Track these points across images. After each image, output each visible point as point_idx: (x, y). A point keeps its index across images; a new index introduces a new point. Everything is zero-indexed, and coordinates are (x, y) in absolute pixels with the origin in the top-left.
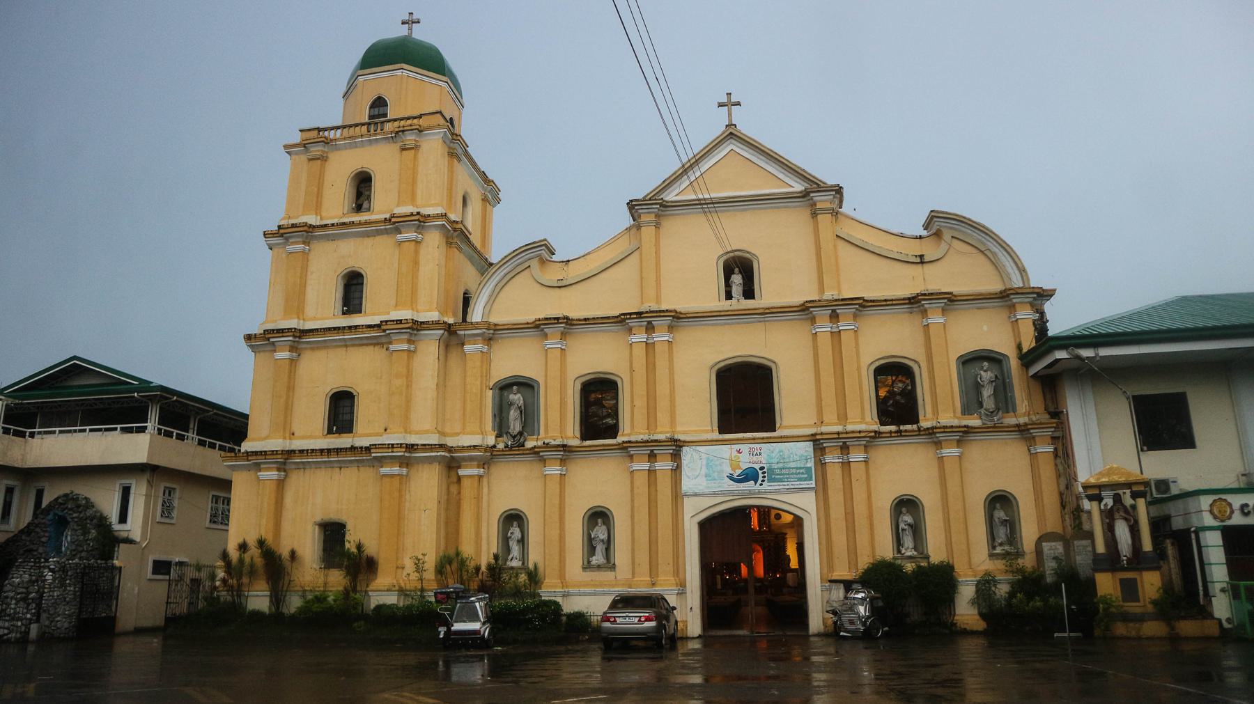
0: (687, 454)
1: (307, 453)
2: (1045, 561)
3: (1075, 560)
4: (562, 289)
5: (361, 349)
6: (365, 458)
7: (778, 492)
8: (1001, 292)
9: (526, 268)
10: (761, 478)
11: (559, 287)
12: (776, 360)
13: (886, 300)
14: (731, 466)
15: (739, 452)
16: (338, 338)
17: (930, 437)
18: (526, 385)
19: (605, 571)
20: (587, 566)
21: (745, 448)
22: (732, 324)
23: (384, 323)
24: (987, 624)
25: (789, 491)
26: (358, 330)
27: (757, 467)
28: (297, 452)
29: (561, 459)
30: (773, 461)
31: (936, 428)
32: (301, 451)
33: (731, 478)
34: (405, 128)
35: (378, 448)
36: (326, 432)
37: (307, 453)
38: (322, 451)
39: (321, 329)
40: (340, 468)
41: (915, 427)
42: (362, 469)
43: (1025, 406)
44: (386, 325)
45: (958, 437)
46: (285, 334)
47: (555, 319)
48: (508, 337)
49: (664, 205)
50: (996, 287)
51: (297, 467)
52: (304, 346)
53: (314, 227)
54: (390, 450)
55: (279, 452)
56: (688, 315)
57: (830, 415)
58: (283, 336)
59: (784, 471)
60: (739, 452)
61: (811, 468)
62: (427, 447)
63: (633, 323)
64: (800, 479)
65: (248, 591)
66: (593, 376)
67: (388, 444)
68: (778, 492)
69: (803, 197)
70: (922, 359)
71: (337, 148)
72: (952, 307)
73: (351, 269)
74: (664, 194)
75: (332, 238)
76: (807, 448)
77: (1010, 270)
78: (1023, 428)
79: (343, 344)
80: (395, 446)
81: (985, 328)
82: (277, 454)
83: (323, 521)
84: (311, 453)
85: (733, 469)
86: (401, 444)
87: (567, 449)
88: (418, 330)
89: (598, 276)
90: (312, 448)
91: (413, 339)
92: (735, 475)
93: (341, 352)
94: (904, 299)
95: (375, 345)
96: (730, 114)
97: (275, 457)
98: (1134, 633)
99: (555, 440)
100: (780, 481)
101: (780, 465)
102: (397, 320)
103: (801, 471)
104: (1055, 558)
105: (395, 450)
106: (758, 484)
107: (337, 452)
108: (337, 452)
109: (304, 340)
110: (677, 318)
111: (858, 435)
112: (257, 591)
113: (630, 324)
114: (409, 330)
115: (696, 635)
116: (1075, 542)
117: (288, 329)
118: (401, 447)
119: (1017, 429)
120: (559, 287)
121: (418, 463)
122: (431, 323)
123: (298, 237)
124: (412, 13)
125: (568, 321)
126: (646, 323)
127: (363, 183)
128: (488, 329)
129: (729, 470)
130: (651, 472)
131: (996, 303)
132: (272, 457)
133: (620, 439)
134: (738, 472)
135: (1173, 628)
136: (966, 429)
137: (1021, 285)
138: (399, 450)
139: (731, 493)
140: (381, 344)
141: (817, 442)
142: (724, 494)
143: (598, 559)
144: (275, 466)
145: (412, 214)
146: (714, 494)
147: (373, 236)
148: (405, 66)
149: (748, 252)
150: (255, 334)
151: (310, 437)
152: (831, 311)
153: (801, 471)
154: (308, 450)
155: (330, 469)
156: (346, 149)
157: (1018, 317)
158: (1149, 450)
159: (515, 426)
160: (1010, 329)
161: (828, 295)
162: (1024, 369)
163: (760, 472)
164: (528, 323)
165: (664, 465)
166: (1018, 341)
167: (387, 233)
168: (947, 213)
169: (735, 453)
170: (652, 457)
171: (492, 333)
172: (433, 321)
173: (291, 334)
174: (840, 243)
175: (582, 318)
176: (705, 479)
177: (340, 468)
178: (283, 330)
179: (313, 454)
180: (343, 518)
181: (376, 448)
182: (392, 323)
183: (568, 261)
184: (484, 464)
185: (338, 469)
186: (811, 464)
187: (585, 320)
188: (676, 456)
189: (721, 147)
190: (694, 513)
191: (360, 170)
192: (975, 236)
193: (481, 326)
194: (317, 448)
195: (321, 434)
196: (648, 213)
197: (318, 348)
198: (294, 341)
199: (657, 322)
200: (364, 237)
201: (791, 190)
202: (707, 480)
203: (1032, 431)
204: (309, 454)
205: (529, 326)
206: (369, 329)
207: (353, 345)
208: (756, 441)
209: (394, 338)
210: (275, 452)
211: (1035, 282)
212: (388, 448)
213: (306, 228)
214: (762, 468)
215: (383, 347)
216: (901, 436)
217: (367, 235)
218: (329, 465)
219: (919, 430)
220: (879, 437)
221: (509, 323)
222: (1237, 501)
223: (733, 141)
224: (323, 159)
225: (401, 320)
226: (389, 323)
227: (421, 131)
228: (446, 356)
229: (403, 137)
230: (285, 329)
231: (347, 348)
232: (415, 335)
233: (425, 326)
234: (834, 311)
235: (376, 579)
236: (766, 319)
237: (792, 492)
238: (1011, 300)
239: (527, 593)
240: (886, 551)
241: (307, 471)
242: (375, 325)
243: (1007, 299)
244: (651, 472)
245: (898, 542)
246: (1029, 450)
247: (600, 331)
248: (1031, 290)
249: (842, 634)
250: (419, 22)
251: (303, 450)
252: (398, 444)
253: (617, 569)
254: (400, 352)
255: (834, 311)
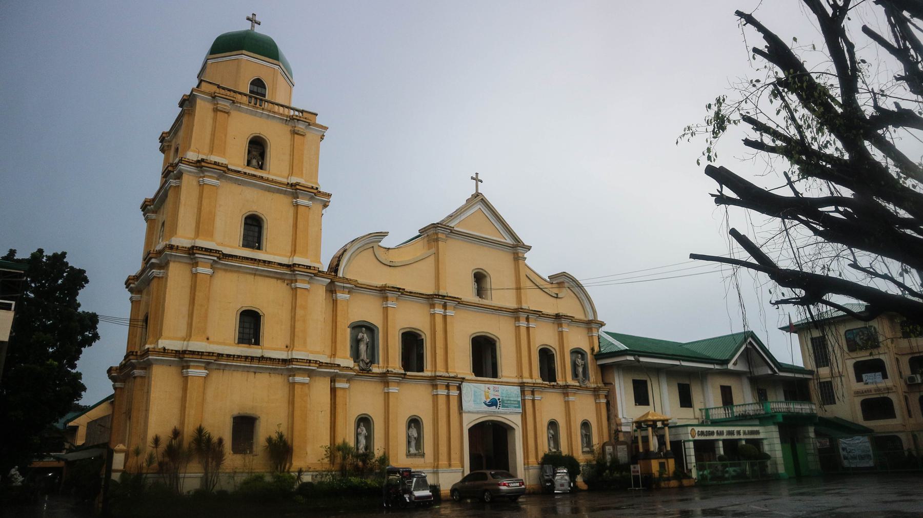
0: (465, 386)
1: (234, 357)
3: (617, 455)
4: (391, 267)
5: (267, 280)
6: (279, 367)
7: (505, 413)
10: (498, 405)
11: (390, 266)
12: (500, 338)
13: (547, 315)
14: (485, 396)
15: (489, 389)
16: (252, 267)
18: (370, 329)
19: (418, 458)
20: (409, 455)
21: (491, 386)
22: (413, 301)
23: (297, 266)
24: (588, 486)
25: (511, 413)
26: (270, 265)
27: (497, 398)
28: (224, 356)
30: (503, 395)
32: (228, 356)
33: (486, 404)
34: (301, 119)
35: (299, 362)
36: (237, 342)
37: (234, 357)
38: (246, 357)
39: (240, 256)
40: (255, 373)
42: (272, 375)
43: (593, 380)
46: (211, 254)
47: (397, 288)
48: (361, 293)
49: (452, 231)
51: (218, 368)
52: (219, 266)
54: (308, 364)
55: (215, 355)
56: (464, 303)
57: (526, 373)
58: (210, 255)
59: (509, 402)
60: (489, 389)
61: (519, 401)
62: (329, 365)
64: (515, 407)
65: (185, 473)
66: (409, 330)
67: (307, 360)
68: (505, 413)
70: (557, 349)
71: (239, 109)
73: (254, 213)
75: (236, 181)
76: (517, 390)
77: (589, 310)
79: (254, 272)
80: (312, 362)
81: (579, 337)
82: (212, 356)
83: (239, 415)
84: (237, 358)
85: (486, 399)
86: (316, 361)
89: (412, 265)
90: (239, 354)
92: (488, 401)
93: (250, 278)
95: (278, 279)
97: (210, 358)
98: (667, 486)
99: (394, 369)
100: (507, 407)
101: (507, 399)
102: (307, 266)
103: (515, 402)
104: (610, 454)
105: (311, 364)
106: (497, 408)
107: (259, 360)
108: (259, 360)
109: (222, 262)
111: (541, 385)
112: (191, 473)
116: (618, 447)
118: (316, 363)
120: (390, 266)
121: (316, 376)
123: (215, 173)
124: (255, 15)
129: (484, 399)
130: (448, 396)
131: (584, 325)
132: (207, 358)
133: (427, 373)
134: (488, 400)
135: (682, 483)
138: (314, 365)
139: (486, 412)
141: (522, 385)
142: (482, 413)
143: (413, 450)
144: (203, 365)
145: (312, 188)
146: (478, 413)
147: (272, 192)
148: (244, 52)
149: (485, 271)
150: (177, 246)
151: (224, 344)
153: (515, 402)
154: (234, 356)
155: (246, 373)
156: (246, 113)
157: (389, 305)
158: (639, 405)
159: (364, 355)
160: (588, 341)
163: (498, 401)
164: (376, 287)
165: (454, 393)
166: (592, 347)
167: (285, 194)
168: (569, 275)
169: (487, 389)
170: (448, 387)
171: (356, 288)
175: (409, 291)
176: (473, 402)
177: (255, 373)
178: (211, 250)
179: (239, 359)
180: (257, 413)
181: (297, 361)
182: (303, 267)
183: (389, 249)
185: (253, 373)
186: (520, 399)
187: (410, 292)
188: (459, 388)
190: (469, 421)
191: (259, 135)
192: (576, 290)
193: (352, 282)
194: (243, 355)
195: (233, 342)
196: (443, 233)
197: (231, 271)
199: (449, 304)
200: (265, 190)
201: (505, 241)
202: (475, 404)
204: (235, 359)
205: (377, 289)
206: (279, 266)
207: (260, 275)
208: (496, 383)
210: (211, 354)
211: (600, 318)
212: (307, 362)
213: (225, 169)
214: (499, 399)
215: (284, 282)
216: (554, 388)
217: (269, 190)
218: (247, 369)
221: (365, 283)
222: (697, 429)
223: (481, 204)
225: (310, 267)
226: (300, 266)
227: (309, 125)
229: (296, 123)
230: (213, 250)
231: (255, 276)
233: (321, 274)
237: (512, 414)
240: (547, 451)
241: (226, 372)
242: (284, 264)
244: (448, 396)
245: (357, 441)
246: (595, 401)
247: (416, 301)
249: (555, 492)
250: (259, 24)
251: (230, 355)
252: (314, 361)
253: (426, 456)
254: (303, 290)
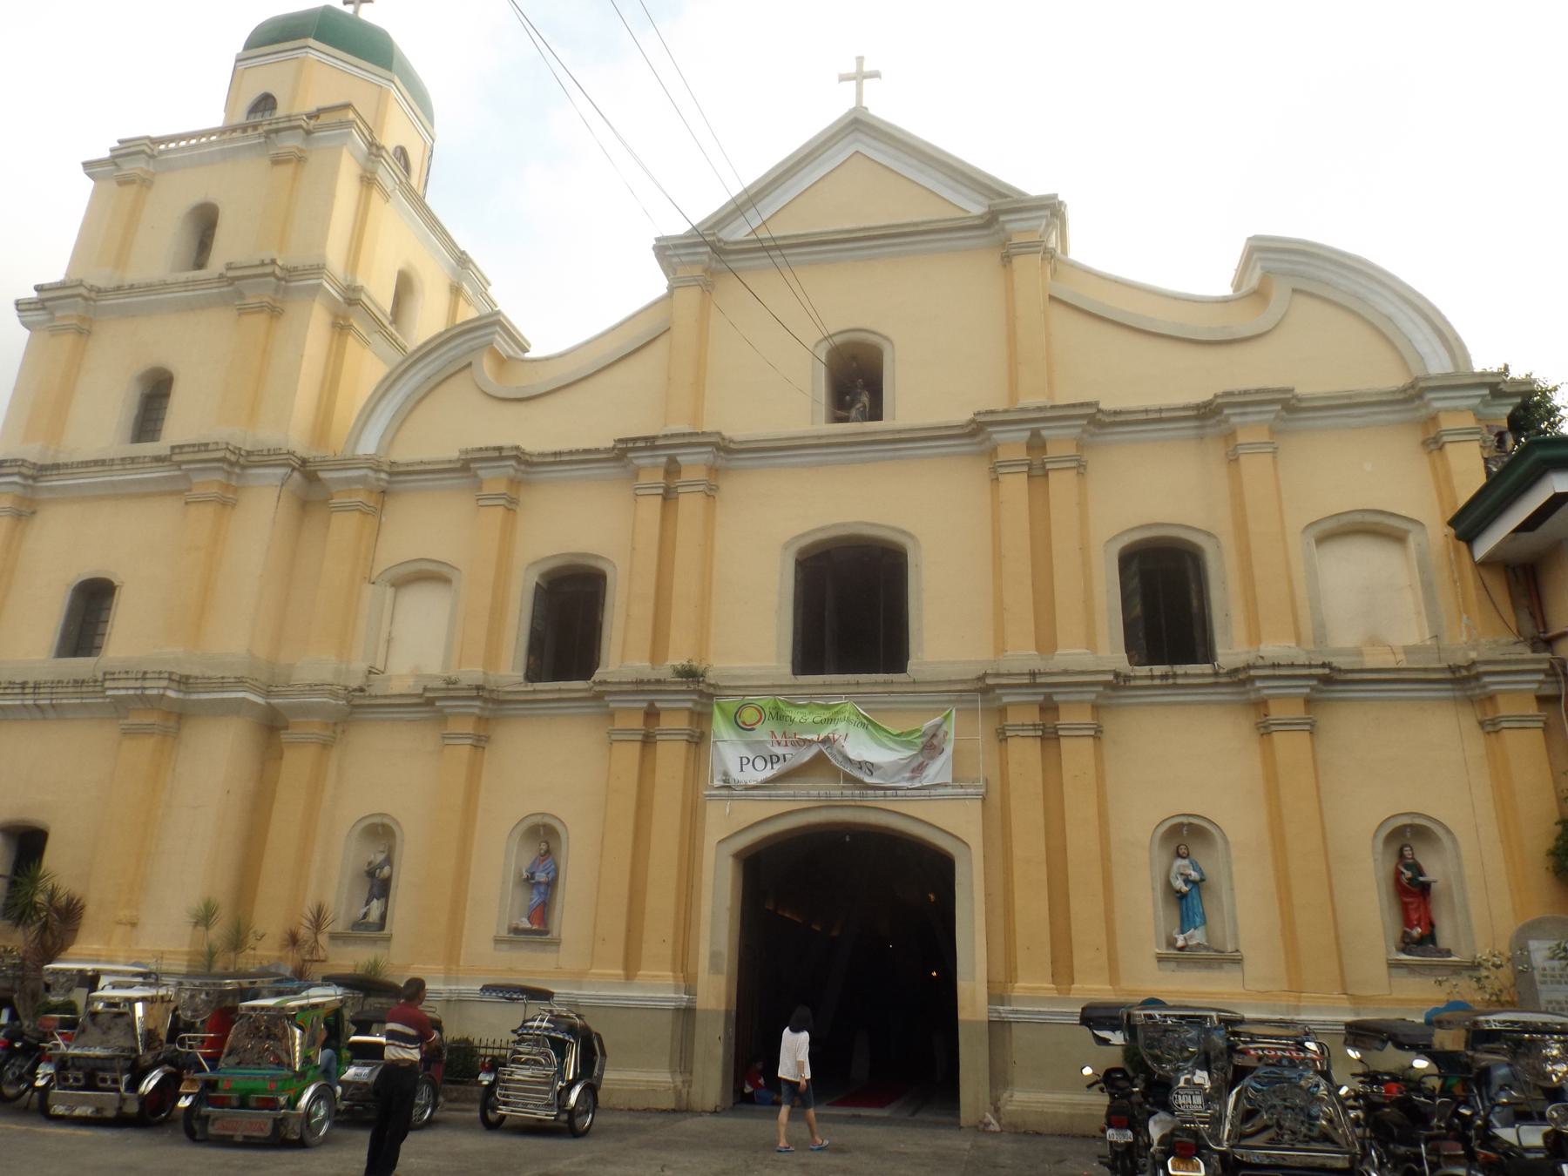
2: (1540, 987)
8: (1404, 390)
9: (460, 370)
17: (1242, 689)
29: (480, 718)
31: (1255, 667)
41: (1206, 668)
44: (181, 453)
45: (1307, 690)
50: (1393, 380)
53: (99, 291)
63: (642, 460)
69: (972, 434)
72: (1115, 701)
74: (728, 229)
78: (1464, 673)
87: (485, 694)
88: (244, 467)
91: (234, 483)
94: (1185, 408)
96: (859, 94)
110: (726, 452)
113: (636, 462)
114: (220, 465)
115: (710, 1106)
117: (11, 461)
119: (1448, 675)
122: (265, 453)
125: (520, 458)
126: (664, 460)
127: (205, 223)
128: (377, 471)
136: (1327, 671)
137: (1450, 369)
140: (179, 493)
149: (874, 333)
152: (1028, 434)
161: (1031, 399)
162: (1463, 545)
172: (269, 450)
173: (16, 470)
174: (1057, 312)
182: (191, 449)
184: (335, 724)
189: (834, 149)
198: (25, 486)
203: (1487, 679)
206: (154, 464)
209: (197, 479)
219: (1216, 674)
220: (1125, 688)
224: (146, 183)
228: (395, 598)
232: (239, 476)
234: (1035, 434)
235: (71, 943)
236: (898, 453)
238: (1426, 406)
239: (501, 992)
243: (1417, 403)
248: (1477, 380)
255: (1035, 434)
